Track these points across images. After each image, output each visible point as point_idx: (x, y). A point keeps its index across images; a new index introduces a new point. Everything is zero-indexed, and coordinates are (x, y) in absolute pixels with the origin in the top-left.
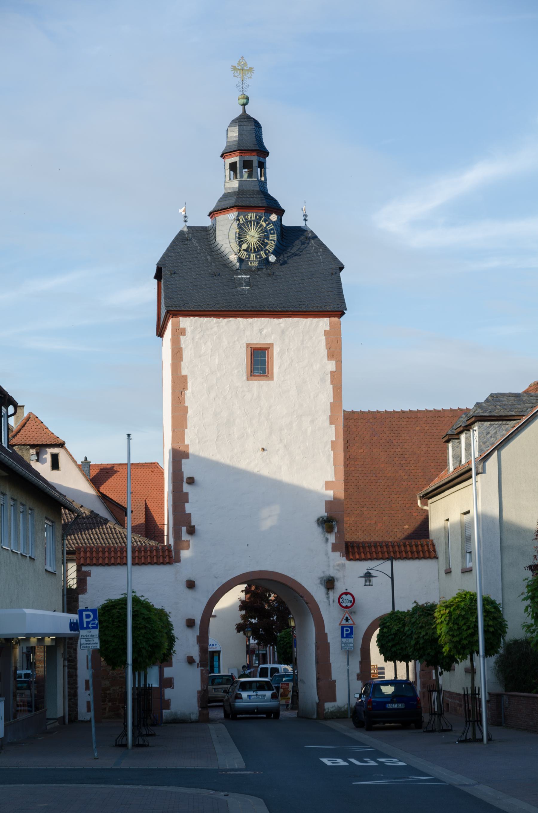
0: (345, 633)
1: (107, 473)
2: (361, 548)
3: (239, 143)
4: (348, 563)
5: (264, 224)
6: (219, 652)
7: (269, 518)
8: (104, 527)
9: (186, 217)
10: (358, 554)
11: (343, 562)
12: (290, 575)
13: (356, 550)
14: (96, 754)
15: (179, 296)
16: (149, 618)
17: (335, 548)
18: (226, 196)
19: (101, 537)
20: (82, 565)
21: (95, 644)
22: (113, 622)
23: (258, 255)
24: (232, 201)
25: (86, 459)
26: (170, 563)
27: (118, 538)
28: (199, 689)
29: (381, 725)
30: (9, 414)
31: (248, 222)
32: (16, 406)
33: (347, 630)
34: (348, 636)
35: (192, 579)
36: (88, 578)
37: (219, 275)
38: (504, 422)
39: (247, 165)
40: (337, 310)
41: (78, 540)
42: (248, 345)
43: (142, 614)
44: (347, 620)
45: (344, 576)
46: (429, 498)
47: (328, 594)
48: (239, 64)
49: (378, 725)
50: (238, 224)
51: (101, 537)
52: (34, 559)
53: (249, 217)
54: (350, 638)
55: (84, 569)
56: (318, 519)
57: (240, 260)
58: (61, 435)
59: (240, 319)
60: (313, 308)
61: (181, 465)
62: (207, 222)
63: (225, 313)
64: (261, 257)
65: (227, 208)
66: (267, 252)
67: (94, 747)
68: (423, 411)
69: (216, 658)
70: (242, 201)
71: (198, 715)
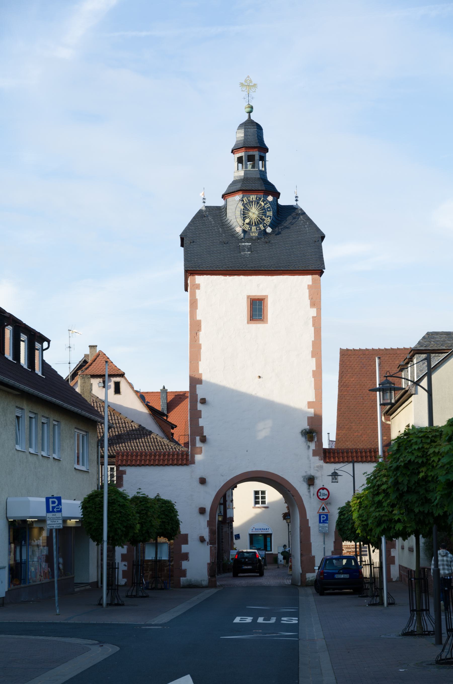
0: (322, 519)
1: (180, 398)
2: (336, 453)
3: (244, 142)
4: (325, 465)
5: (263, 204)
6: (271, 535)
7: (264, 430)
8: (149, 437)
9: (204, 199)
10: (333, 458)
11: (321, 464)
12: (280, 474)
13: (332, 455)
14: (58, 611)
15: (196, 259)
16: (124, 505)
17: (315, 453)
18: (234, 182)
19: (145, 445)
20: (120, 465)
21: (58, 524)
22: (96, 508)
23: (258, 227)
24: (238, 187)
25: (164, 388)
26: (186, 464)
27: (158, 445)
28: (209, 562)
29: (331, 591)
30: (44, 348)
31: (250, 202)
32: (49, 341)
33: (323, 517)
34: (324, 522)
35: (204, 477)
36: (124, 476)
37: (228, 243)
38: (437, 355)
39: (251, 158)
40: (317, 269)
41: (128, 447)
42: (248, 297)
43: (118, 501)
44: (323, 509)
45: (322, 475)
46: (391, 415)
47: (309, 489)
48: (246, 81)
49: (328, 591)
50: (243, 204)
51: (145, 445)
52: (60, 460)
53: (251, 198)
54: (326, 523)
55: (121, 468)
56: (302, 431)
57: (244, 231)
58: (122, 368)
59: (242, 277)
60: (298, 267)
61: (196, 389)
62: (220, 203)
63: (230, 272)
64: (260, 229)
65: (234, 192)
66: (265, 225)
67: (56, 606)
68: (402, 349)
69: (268, 539)
70: (245, 186)
71: (207, 582)
